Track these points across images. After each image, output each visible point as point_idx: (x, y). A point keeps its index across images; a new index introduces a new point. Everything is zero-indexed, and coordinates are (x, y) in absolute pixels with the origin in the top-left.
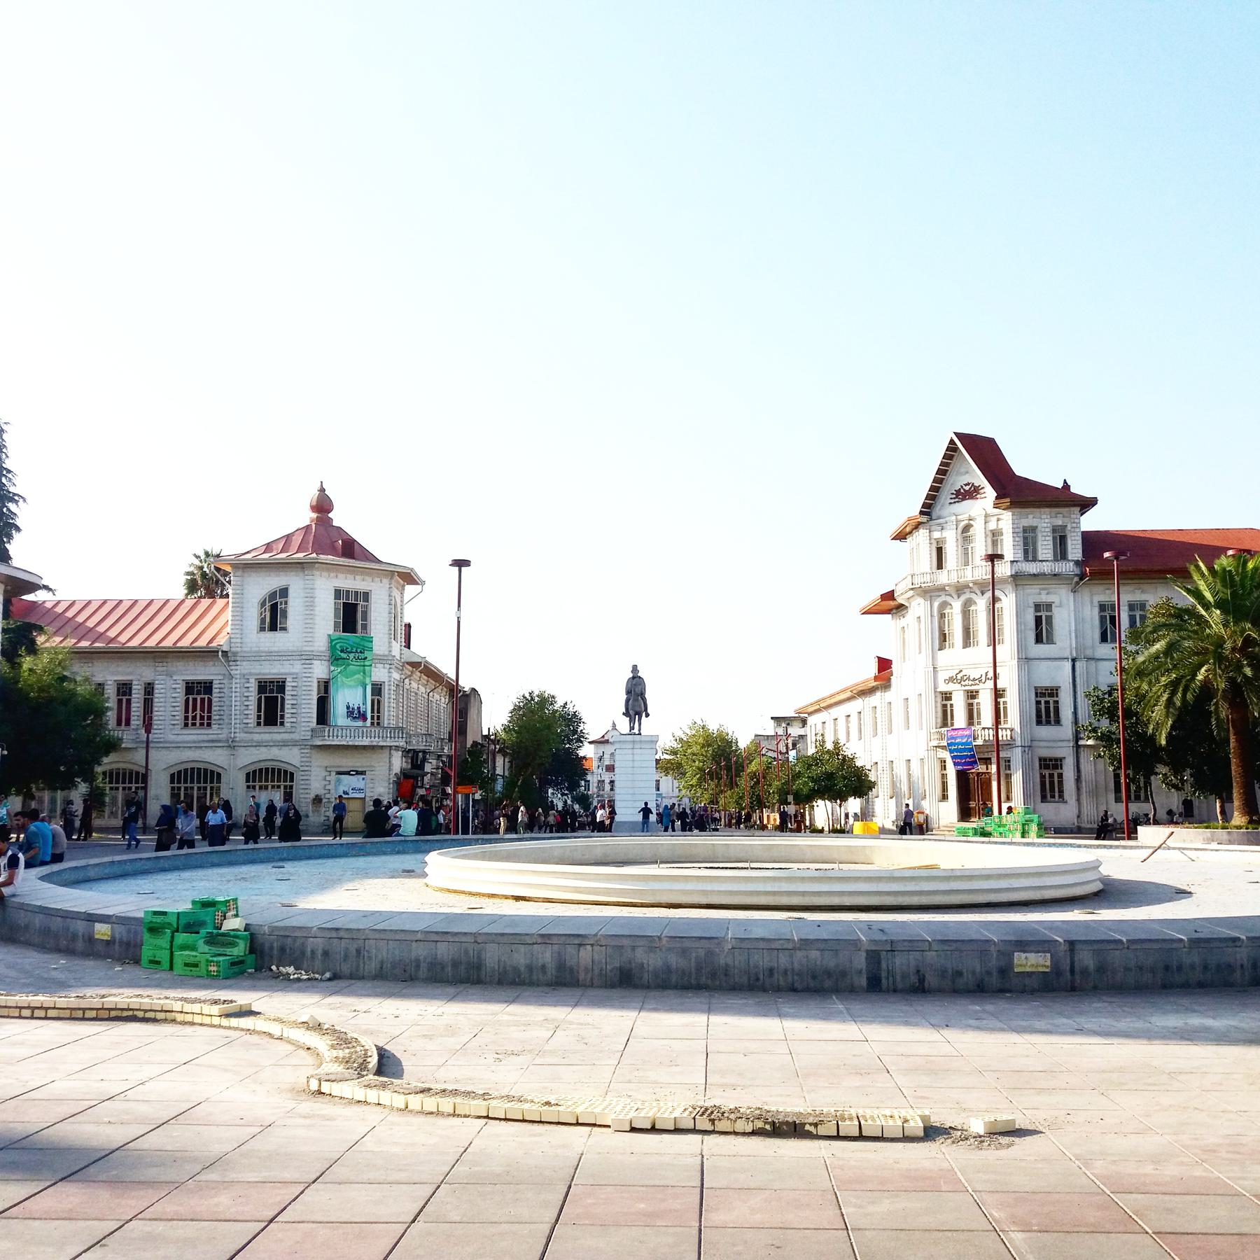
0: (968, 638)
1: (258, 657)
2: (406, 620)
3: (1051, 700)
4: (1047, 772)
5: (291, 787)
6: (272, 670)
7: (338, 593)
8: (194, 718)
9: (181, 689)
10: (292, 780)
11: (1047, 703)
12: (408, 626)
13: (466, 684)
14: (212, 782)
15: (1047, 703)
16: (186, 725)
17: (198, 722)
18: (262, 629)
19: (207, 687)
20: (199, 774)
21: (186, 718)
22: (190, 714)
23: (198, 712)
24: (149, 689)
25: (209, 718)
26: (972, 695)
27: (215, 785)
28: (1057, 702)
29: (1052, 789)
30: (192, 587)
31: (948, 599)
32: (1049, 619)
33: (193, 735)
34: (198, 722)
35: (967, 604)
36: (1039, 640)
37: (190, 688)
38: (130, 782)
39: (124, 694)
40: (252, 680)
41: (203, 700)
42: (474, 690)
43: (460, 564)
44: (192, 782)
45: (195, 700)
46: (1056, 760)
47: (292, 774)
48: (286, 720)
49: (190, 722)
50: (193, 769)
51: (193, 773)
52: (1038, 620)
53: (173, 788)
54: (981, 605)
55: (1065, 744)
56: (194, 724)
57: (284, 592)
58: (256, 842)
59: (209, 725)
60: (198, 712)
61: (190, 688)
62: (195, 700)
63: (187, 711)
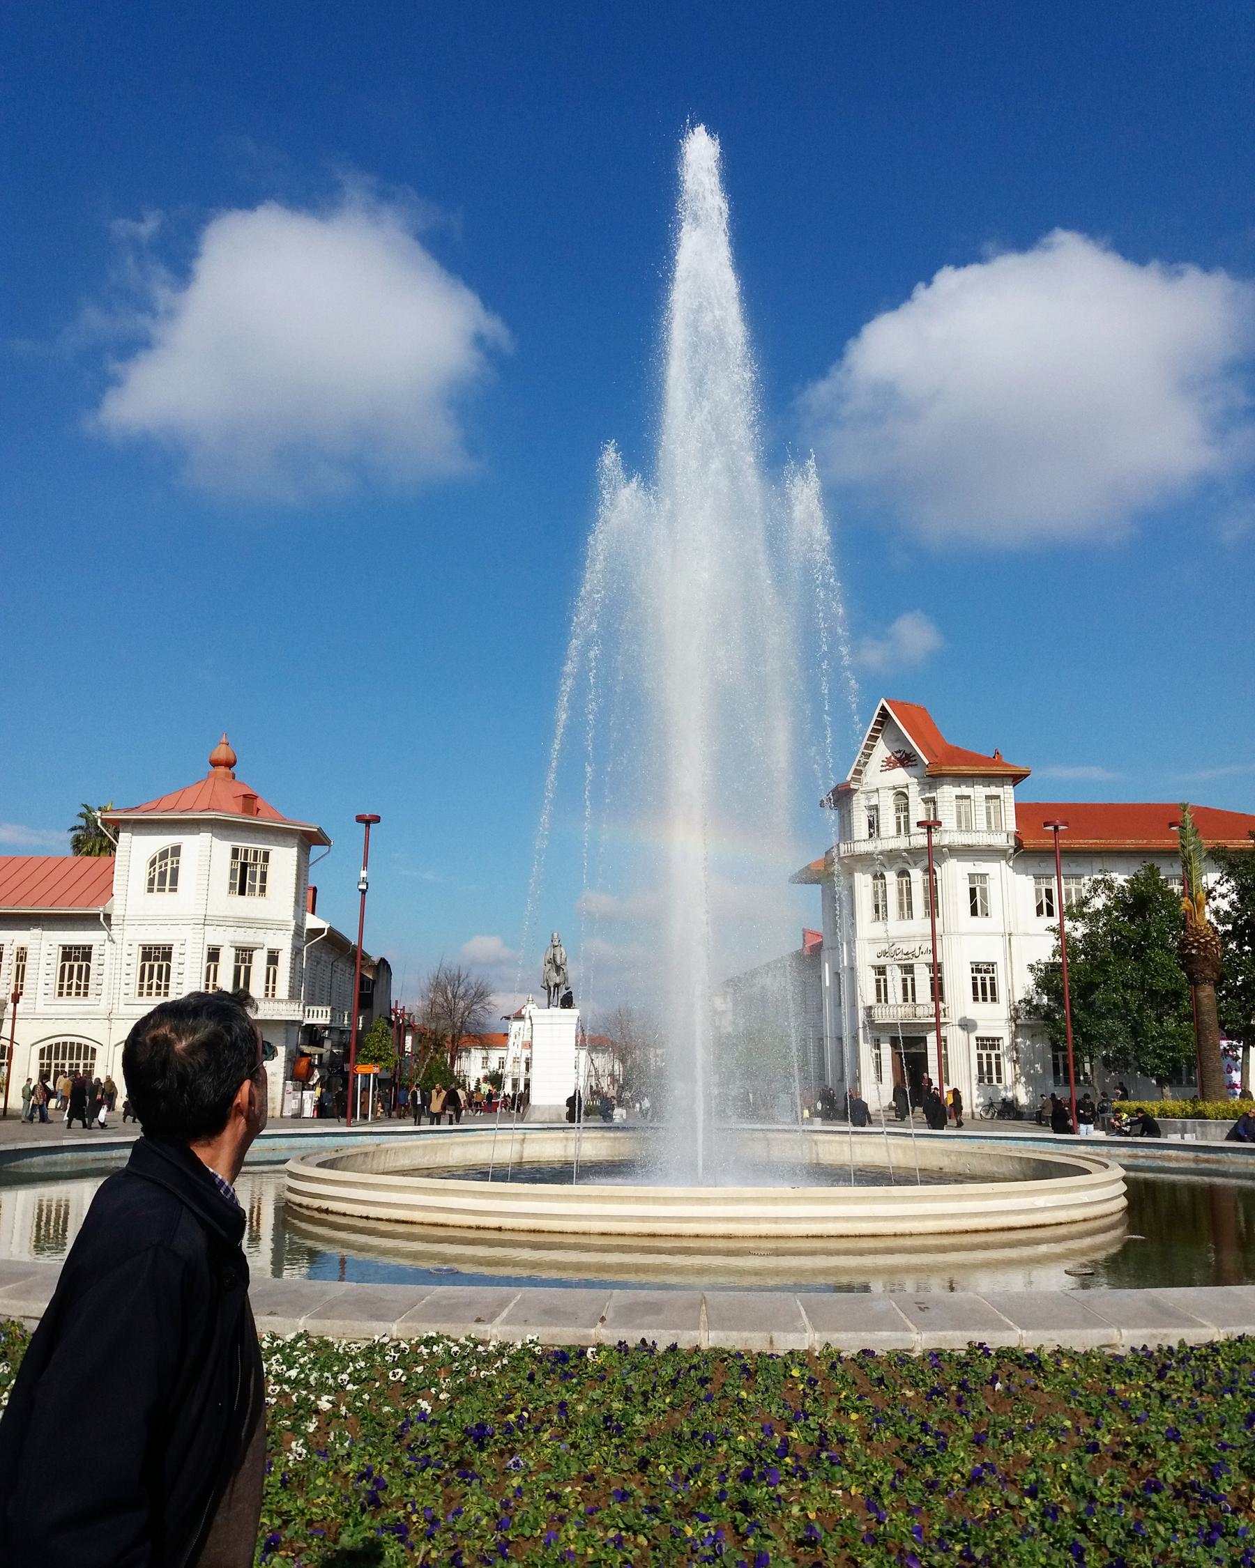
0: (906, 908)
1: (142, 922)
2: (311, 884)
3: (988, 976)
4: (984, 1053)
5: (92, 1065)
6: (157, 937)
7: (235, 853)
8: (150, 987)
9: (137, 953)
10: (93, 1058)
11: (983, 979)
12: (315, 890)
13: (374, 951)
14: (71, 1058)
15: (983, 979)
16: (61, 994)
17: (74, 991)
18: (151, 890)
19: (166, 953)
20: (72, 1049)
21: (61, 987)
22: (66, 983)
23: (75, 980)
24: (22, 955)
25: (86, 987)
26: (909, 969)
27: (89, 1061)
28: (992, 979)
29: (984, 992)
30: (78, 845)
31: (906, 866)
32: (984, 891)
33: (72, 1005)
34: (74, 991)
35: (903, 873)
36: (974, 912)
37: (68, 953)
38: (64, 1058)
39: (244, 961)
40: (136, 945)
41: (80, 967)
42: (383, 961)
43: (368, 821)
44: (64, 1058)
45: (72, 967)
46: (993, 1039)
47: (94, 1050)
48: (170, 991)
49: (65, 991)
50: (65, 1044)
51: (72, 1049)
52: (973, 892)
53: (42, 1065)
54: (917, 875)
55: (998, 1023)
56: (78, 994)
57: (176, 851)
58: (438, 1124)
59: (86, 994)
60: (75, 980)
61: (68, 953)
62: (72, 967)
63: (62, 979)
